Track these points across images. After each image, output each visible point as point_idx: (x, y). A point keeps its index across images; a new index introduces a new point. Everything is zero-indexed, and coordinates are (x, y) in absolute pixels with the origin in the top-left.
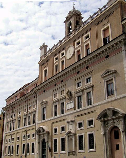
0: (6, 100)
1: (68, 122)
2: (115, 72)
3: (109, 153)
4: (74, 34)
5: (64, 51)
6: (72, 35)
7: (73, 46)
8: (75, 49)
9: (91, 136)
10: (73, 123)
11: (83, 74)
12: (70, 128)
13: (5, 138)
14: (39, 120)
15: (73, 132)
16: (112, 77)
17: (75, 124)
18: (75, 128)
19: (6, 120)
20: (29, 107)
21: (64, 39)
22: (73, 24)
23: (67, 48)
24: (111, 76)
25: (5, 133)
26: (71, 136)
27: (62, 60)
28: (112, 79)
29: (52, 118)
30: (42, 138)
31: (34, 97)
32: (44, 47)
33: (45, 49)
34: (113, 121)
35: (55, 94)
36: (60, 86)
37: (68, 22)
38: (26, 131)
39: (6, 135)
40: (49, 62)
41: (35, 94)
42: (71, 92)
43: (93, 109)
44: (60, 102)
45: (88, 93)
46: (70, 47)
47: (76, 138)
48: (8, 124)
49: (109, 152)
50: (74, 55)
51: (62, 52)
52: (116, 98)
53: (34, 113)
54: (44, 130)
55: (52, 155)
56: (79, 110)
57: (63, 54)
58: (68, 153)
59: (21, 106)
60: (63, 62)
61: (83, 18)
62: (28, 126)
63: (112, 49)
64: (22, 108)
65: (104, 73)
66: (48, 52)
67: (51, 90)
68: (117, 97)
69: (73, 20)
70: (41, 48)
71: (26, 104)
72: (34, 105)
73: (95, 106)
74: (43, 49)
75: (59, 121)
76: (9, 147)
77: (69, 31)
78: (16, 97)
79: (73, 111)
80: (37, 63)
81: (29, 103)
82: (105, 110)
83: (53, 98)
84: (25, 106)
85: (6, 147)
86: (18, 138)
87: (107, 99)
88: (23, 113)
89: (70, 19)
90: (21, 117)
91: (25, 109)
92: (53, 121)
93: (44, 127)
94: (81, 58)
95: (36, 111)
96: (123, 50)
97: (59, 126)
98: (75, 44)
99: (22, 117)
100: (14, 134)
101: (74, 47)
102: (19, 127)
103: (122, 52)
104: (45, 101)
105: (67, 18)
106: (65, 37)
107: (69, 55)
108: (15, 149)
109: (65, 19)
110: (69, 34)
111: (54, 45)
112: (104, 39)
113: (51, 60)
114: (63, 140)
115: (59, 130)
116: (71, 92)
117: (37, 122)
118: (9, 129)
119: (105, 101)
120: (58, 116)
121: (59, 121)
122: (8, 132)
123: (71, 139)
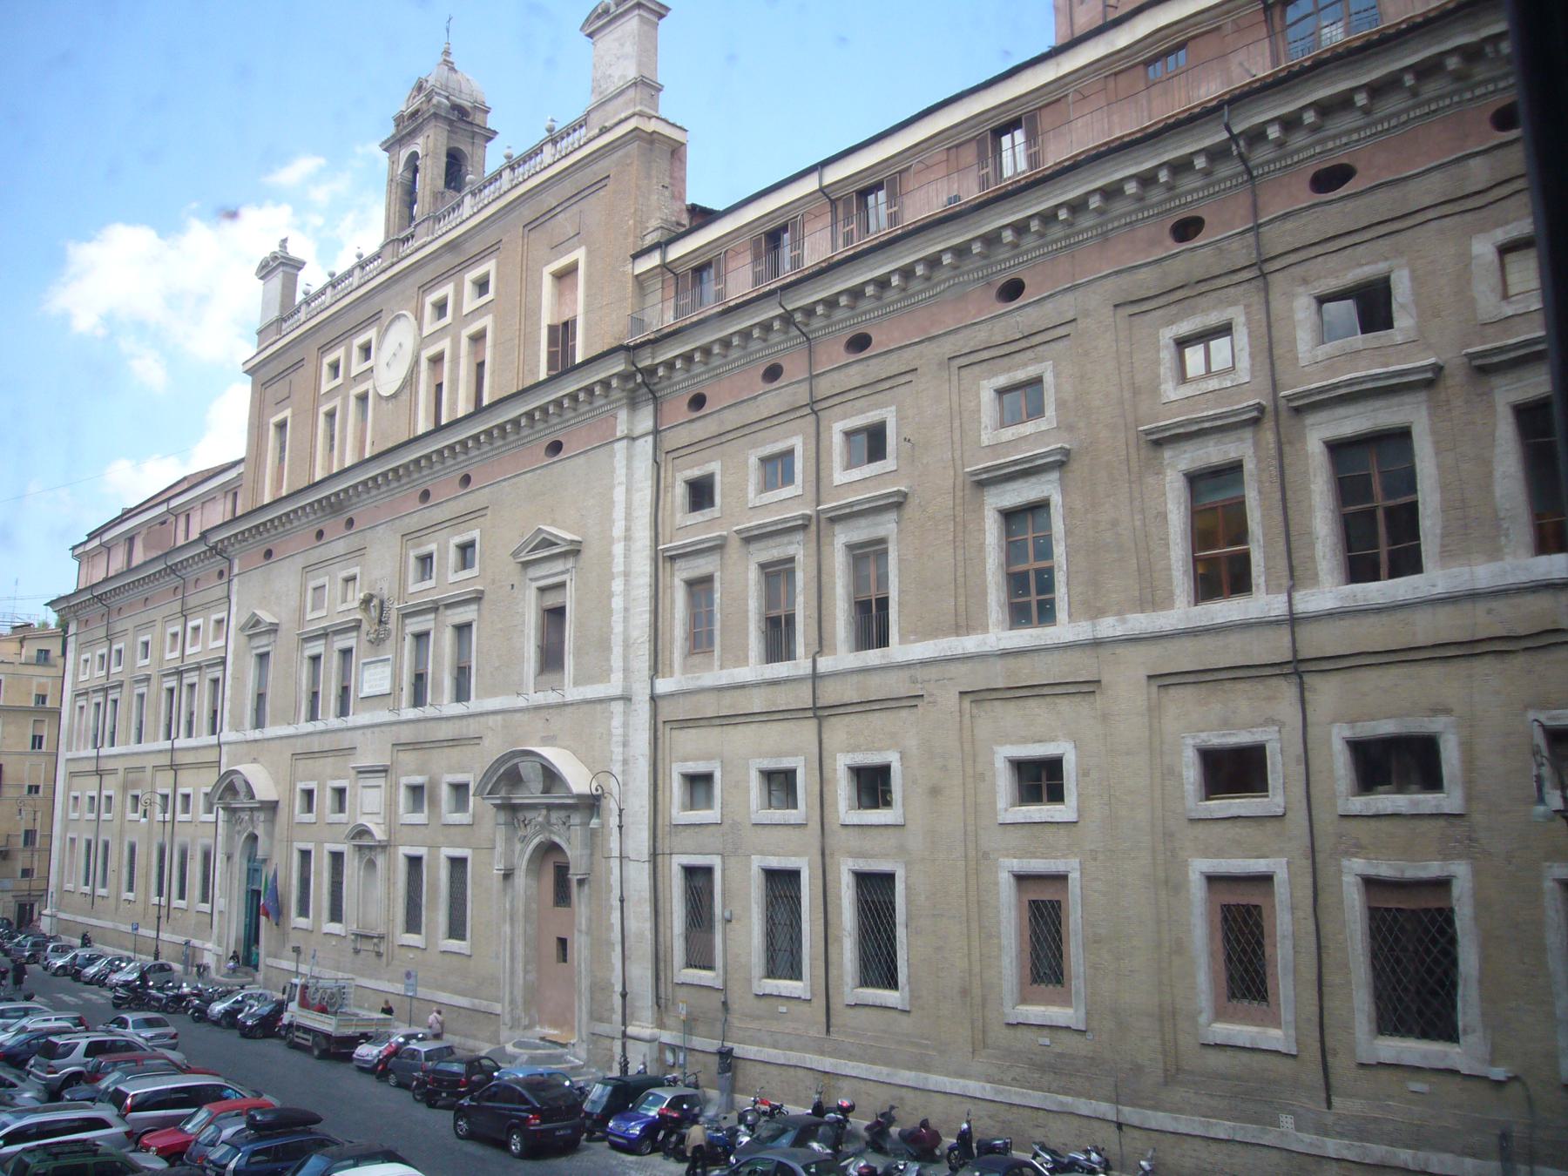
0: (74, 548)
1: (361, 771)
2: (574, 551)
3: (521, 975)
4: (428, 242)
5: (371, 334)
6: (417, 245)
7: (411, 317)
8: (423, 342)
9: (875, 891)
10: (380, 781)
11: (732, 419)
12: (370, 806)
13: (69, 788)
14: (237, 726)
15: (379, 834)
16: (563, 573)
17: (394, 787)
18: (391, 804)
19: (76, 675)
20: (191, 624)
21: (377, 256)
22: (431, 175)
23: (386, 320)
24: (558, 566)
25: (69, 755)
26: (370, 848)
27: (474, 328)
28: (562, 585)
29: (290, 730)
30: (536, 841)
31: (221, 574)
32: (281, 266)
33: (284, 286)
34: (547, 818)
35: (315, 589)
36: (340, 547)
37: (404, 154)
38: (174, 767)
39: (75, 767)
40: (296, 377)
41: (218, 551)
42: (382, 603)
43: (472, 728)
44: (341, 642)
45: (691, 584)
46: (398, 317)
47: (391, 868)
48: (82, 702)
49: (526, 972)
50: (410, 381)
51: (360, 340)
52: (569, 698)
53: (217, 673)
54: (551, 777)
55: (284, 937)
56: (459, 709)
57: (366, 350)
58: (355, 941)
59: (156, 614)
60: (363, 398)
61: (495, 133)
62: (182, 742)
63: (587, 408)
64: (159, 625)
65: (525, 544)
66: (497, 176)
67: (300, 561)
68: (572, 693)
69: (429, 145)
70: (265, 271)
71: (177, 607)
72: (219, 622)
73: (481, 714)
74: (277, 281)
75: (323, 753)
76: (89, 843)
77: (407, 211)
78: (774, 238)
79: (384, 716)
80: (241, 369)
81: (192, 601)
82: (514, 754)
83: (406, 581)
84: (167, 619)
85: (73, 840)
86: (309, 794)
87: (1070, 615)
88: (162, 658)
89: (412, 134)
90: (148, 679)
91: (175, 635)
92: (300, 746)
93: (557, 757)
94: (579, 360)
95: (223, 662)
96: (619, 434)
97: (324, 782)
98: (423, 306)
99: (154, 681)
100: (114, 771)
101: (420, 328)
102: (139, 741)
103: (618, 446)
104: (267, 617)
105: (399, 120)
106: (383, 247)
107: (388, 379)
108: (119, 859)
109: (390, 130)
110: (403, 235)
111: (332, 275)
112: (552, 329)
113: (308, 369)
114: (337, 857)
115: (325, 800)
116: (382, 603)
117: (227, 735)
118: (133, 731)
119: (520, 702)
120: (428, 711)
121: (323, 753)
122: (83, 754)
123: (371, 864)
